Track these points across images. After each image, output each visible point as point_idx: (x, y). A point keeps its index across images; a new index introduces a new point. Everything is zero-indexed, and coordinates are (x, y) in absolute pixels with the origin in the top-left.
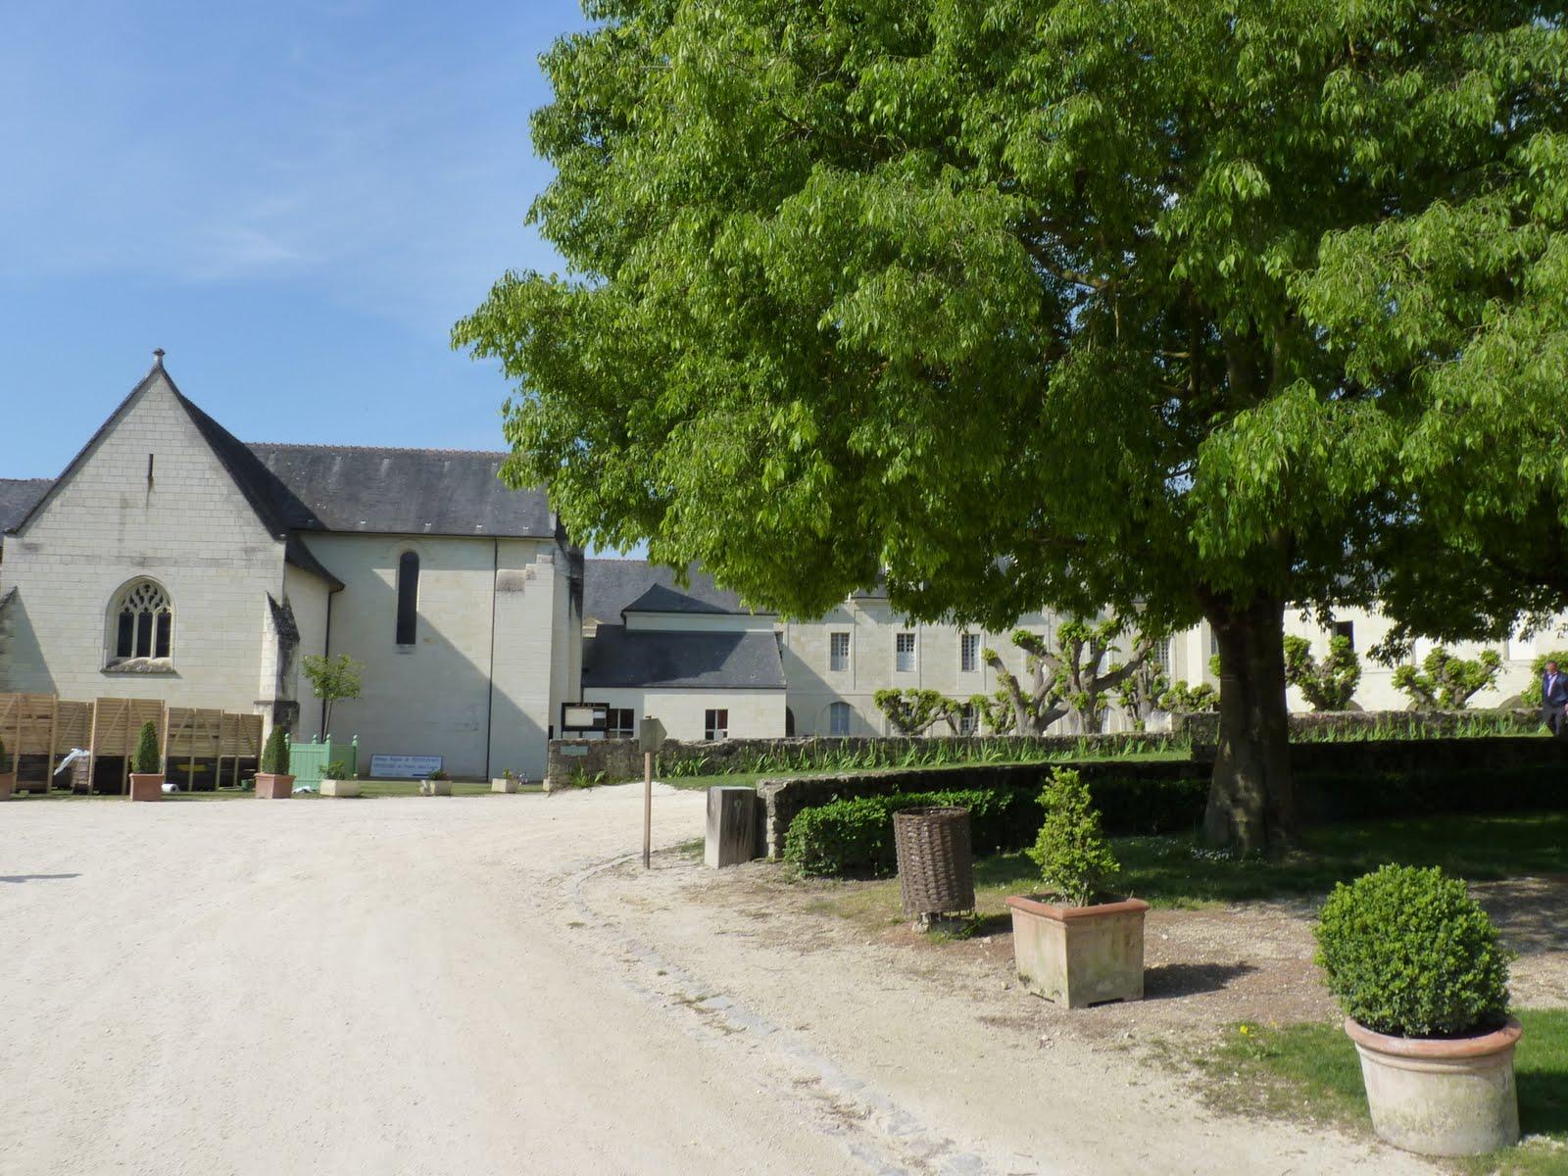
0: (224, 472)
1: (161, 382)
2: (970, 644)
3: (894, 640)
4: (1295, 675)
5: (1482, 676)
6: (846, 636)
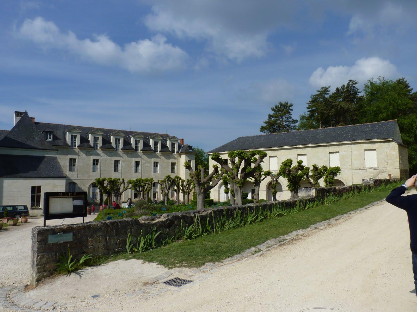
3: (92, 161)
6: (75, 160)
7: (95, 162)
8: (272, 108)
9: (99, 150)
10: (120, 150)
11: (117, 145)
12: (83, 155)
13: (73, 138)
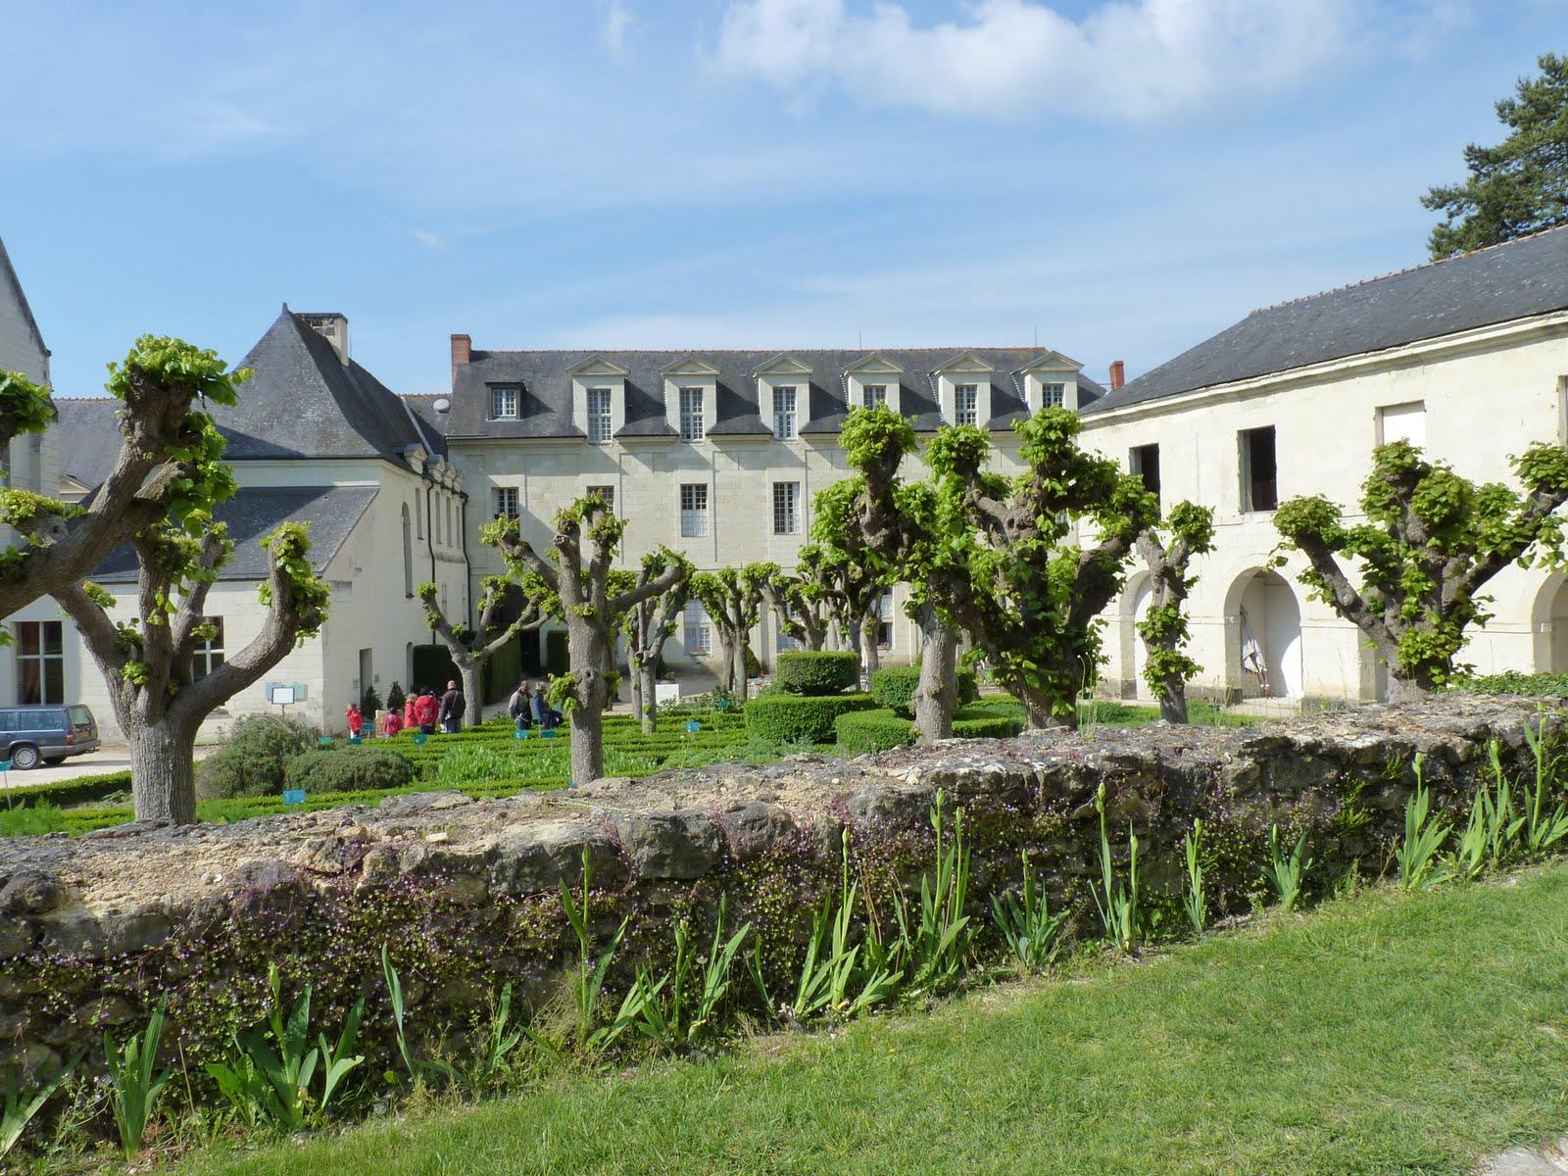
2: (786, 496)
4: (892, 543)
5: (1521, 523)
7: (782, 493)
8: (1501, 110)
9: (796, 444)
10: (797, 437)
11: (781, 417)
12: (638, 469)
13: (598, 400)
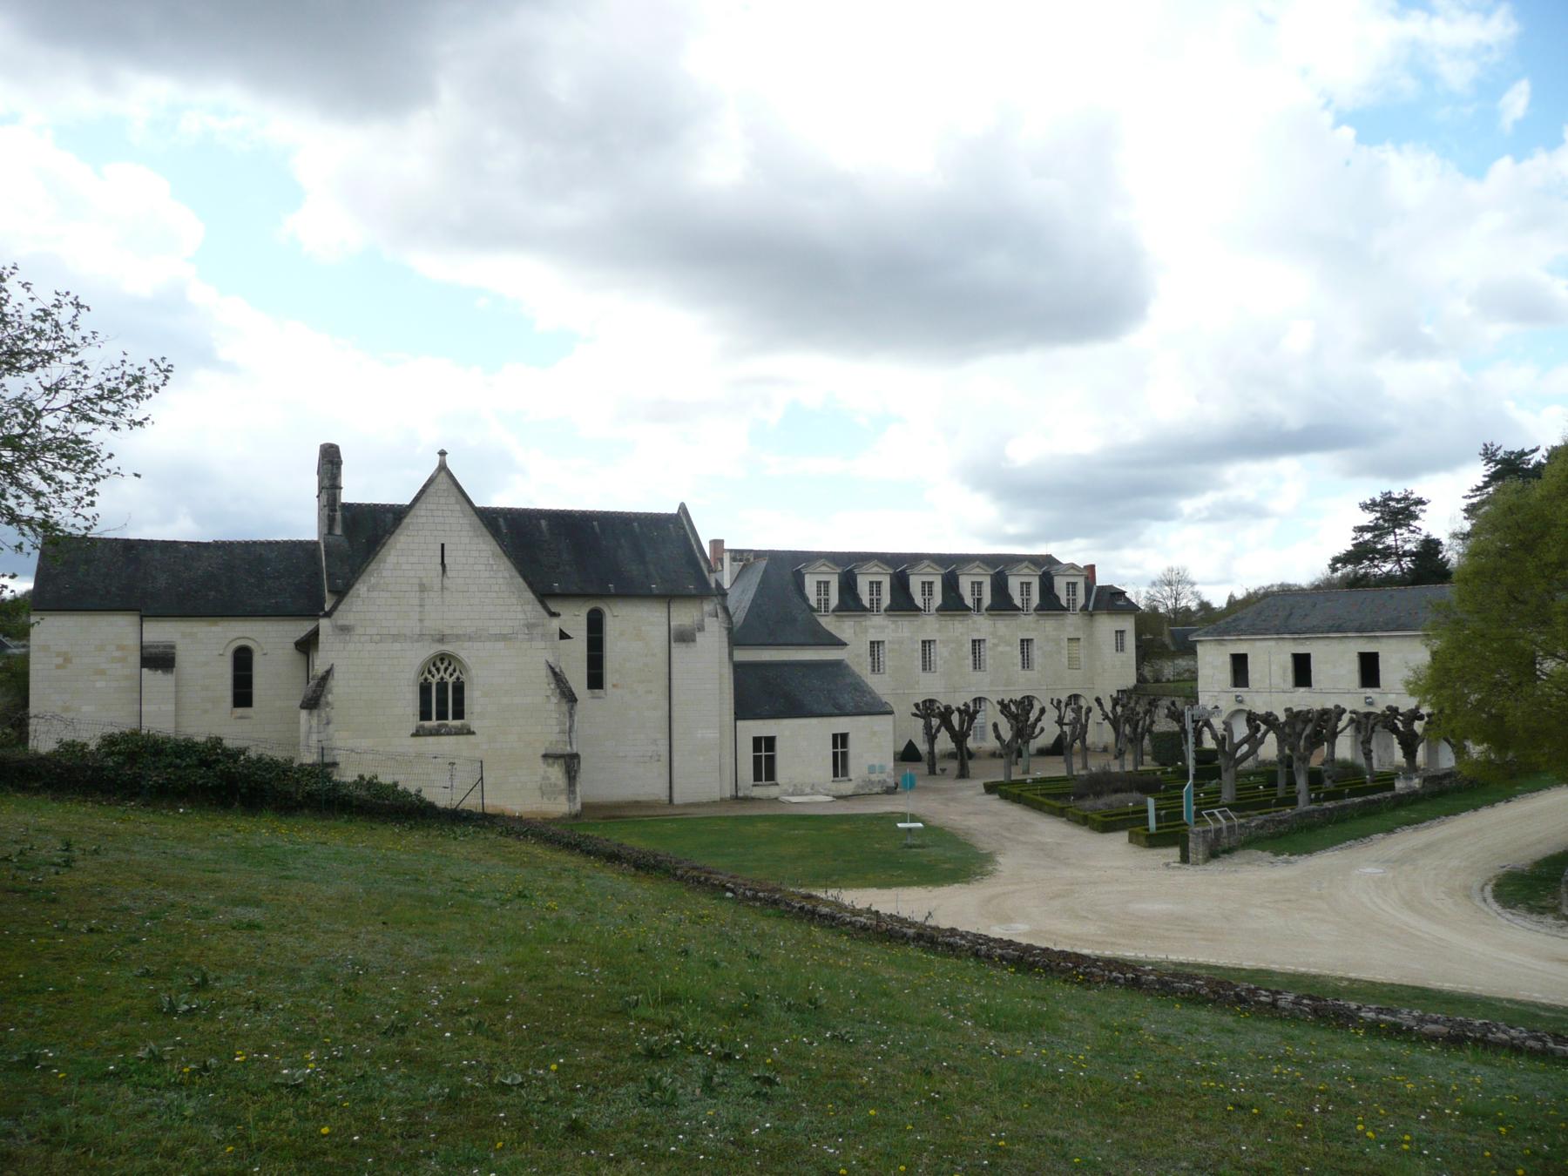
0: (505, 559)
1: (443, 474)
